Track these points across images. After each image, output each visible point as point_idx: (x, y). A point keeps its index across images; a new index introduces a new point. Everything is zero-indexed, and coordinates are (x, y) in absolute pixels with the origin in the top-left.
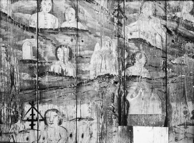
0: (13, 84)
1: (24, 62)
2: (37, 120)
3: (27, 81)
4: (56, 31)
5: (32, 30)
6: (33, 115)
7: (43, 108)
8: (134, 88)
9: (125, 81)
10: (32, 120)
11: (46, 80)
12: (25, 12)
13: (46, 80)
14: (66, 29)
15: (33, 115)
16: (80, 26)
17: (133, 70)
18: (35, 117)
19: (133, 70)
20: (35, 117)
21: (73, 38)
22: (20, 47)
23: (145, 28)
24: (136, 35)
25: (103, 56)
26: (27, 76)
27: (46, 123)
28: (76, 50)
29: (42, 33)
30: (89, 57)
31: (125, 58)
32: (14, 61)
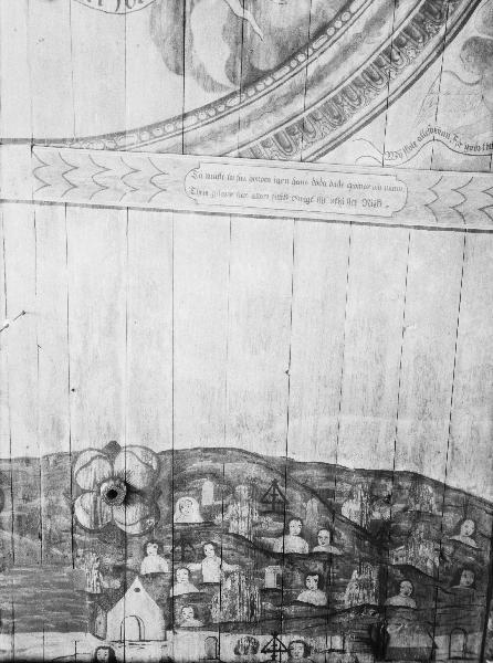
0: (252, 614)
1: (267, 590)
2: (280, 650)
3: (270, 611)
4: (303, 557)
5: (275, 555)
6: (275, 645)
7: (285, 640)
8: (53, 649)
9: (384, 611)
10: (274, 651)
11: (290, 610)
12: (269, 535)
13: (290, 610)
14: (317, 553)
15: (275, 645)
16: (335, 551)
17: (397, 601)
18: (278, 648)
19: (397, 601)
20: (278, 648)
21: (443, 620)
22: (263, 576)
23: (295, 71)
24: (402, 561)
25: (363, 585)
26: (269, 606)
27: (290, 655)
28: (329, 577)
29: (286, 558)
30: (344, 586)
31: (387, 585)
32: (255, 590)
